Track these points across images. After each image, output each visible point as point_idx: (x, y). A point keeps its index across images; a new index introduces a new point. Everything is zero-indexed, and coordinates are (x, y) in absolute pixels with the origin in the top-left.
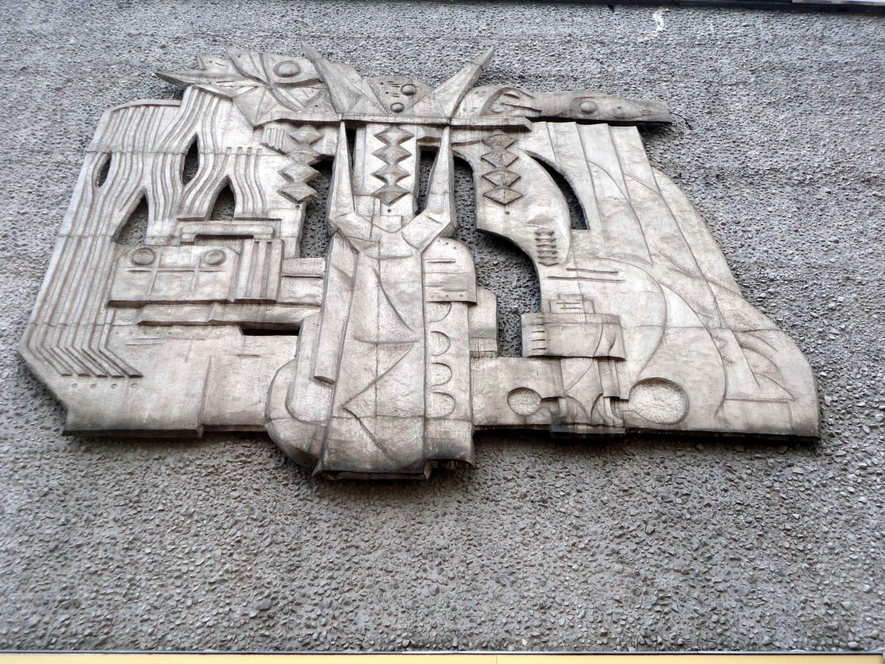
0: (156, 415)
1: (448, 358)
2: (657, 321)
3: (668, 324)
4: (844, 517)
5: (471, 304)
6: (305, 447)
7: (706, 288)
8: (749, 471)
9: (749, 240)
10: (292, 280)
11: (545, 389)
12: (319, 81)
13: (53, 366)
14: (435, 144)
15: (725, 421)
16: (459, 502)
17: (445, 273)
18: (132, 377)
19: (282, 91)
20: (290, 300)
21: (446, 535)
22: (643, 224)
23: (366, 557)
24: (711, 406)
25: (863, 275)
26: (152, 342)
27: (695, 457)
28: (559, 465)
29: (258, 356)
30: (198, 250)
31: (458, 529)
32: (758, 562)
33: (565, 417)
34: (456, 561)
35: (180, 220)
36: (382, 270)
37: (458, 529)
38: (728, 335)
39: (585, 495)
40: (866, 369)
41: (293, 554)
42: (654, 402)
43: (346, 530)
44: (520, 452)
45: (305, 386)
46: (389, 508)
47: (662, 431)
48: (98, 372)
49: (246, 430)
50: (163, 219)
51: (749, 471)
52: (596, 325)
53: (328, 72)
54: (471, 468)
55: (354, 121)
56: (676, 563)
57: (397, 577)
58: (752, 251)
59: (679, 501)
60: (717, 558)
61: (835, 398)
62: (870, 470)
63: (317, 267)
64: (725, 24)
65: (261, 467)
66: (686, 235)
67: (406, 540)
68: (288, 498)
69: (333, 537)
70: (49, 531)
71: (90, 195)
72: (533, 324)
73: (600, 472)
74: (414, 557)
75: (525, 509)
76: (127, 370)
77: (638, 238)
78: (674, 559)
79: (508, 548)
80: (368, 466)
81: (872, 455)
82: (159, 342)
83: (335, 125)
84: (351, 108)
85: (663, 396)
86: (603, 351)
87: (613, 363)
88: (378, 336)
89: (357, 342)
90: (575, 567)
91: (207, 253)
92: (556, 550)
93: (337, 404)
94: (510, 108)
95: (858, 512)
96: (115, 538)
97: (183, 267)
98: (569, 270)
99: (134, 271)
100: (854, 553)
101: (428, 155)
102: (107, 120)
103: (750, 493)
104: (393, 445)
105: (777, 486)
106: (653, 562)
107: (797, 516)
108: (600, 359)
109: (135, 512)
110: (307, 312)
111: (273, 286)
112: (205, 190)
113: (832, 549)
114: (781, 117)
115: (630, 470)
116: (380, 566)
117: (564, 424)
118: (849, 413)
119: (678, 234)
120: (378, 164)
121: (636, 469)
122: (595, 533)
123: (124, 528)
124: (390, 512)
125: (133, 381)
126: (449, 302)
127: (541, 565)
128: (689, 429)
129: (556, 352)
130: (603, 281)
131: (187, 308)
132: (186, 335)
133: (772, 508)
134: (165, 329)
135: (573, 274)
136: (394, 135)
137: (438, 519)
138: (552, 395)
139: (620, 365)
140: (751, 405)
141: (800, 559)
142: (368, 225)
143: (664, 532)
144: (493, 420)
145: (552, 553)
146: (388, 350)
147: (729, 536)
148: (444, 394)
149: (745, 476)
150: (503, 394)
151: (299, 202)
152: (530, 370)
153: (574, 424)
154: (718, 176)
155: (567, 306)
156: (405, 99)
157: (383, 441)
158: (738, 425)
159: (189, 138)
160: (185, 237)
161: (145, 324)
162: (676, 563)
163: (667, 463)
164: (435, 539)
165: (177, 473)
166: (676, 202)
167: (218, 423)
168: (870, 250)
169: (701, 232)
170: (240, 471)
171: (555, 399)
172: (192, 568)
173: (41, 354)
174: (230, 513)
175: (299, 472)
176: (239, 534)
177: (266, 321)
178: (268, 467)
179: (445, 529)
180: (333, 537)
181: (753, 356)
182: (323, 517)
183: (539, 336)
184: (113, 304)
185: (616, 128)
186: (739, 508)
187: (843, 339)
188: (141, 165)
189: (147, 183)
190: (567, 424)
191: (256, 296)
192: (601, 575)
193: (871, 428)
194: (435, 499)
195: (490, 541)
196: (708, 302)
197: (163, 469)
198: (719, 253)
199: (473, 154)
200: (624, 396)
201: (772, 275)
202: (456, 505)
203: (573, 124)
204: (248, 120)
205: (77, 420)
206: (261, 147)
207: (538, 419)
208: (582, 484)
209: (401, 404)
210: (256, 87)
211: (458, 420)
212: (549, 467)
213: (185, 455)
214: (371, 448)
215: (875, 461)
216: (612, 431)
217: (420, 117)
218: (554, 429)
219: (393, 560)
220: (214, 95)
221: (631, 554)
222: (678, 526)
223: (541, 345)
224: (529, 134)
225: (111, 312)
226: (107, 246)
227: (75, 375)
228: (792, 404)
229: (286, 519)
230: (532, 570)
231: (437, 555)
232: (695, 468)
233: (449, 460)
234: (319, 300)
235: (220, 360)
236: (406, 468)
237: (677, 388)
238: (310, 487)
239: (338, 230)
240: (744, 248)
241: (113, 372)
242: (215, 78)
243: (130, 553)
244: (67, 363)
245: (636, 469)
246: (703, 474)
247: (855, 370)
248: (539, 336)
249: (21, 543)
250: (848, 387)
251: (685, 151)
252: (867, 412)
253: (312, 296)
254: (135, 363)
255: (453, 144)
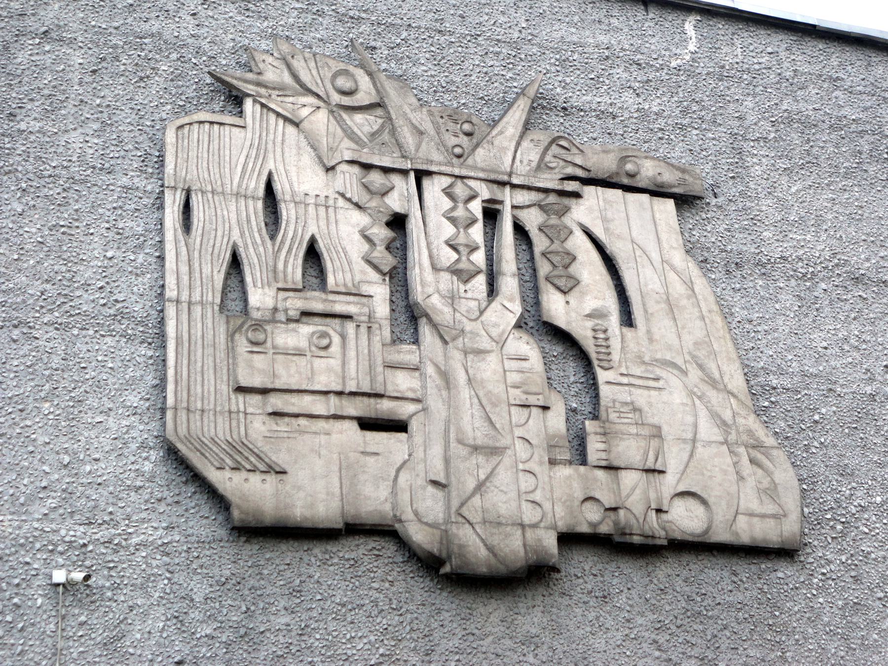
0: (308, 513)
1: (532, 466)
2: (690, 436)
3: (698, 436)
4: (807, 615)
5: (545, 408)
6: (435, 551)
7: (727, 401)
8: (747, 575)
9: (758, 342)
10: (393, 370)
11: (608, 500)
12: (378, 105)
13: (206, 458)
14: (497, 207)
15: (737, 534)
16: (544, 596)
17: (523, 372)
18: (277, 473)
19: (345, 116)
20: (396, 394)
21: (536, 624)
22: (679, 326)
23: (481, 642)
24: (728, 520)
25: (842, 386)
26: (286, 435)
27: (710, 561)
28: (614, 564)
29: (377, 454)
30: (306, 329)
31: (545, 620)
32: (749, 651)
33: (624, 528)
34: (545, 647)
35: (279, 289)
36: (469, 364)
37: (545, 620)
38: (742, 450)
39: (633, 592)
40: (835, 483)
41: (427, 639)
42: (686, 513)
43: (464, 619)
44: (585, 552)
45: (424, 488)
46: (493, 600)
47: (693, 542)
48: (248, 467)
49: (379, 528)
50: (263, 287)
51: (747, 575)
52: (645, 437)
53: (388, 95)
54: (555, 569)
55: (422, 171)
56: (695, 652)
57: (505, 660)
58: (761, 355)
59: (699, 599)
60: (723, 647)
61: (811, 510)
62: (828, 575)
63: (413, 357)
64: (751, 48)
65: (391, 560)
66: (712, 340)
67: (508, 628)
68: (418, 590)
69: (455, 625)
70: (235, 618)
71: (184, 249)
72: (596, 434)
73: (643, 572)
74: (516, 643)
75: (591, 603)
76: (273, 465)
77: (676, 342)
78: (695, 647)
79: (581, 636)
80: (485, 570)
81: (831, 562)
82: (291, 435)
83: (404, 172)
84: (417, 150)
85: (693, 508)
86: (650, 464)
87: (656, 474)
88: (475, 439)
89: (460, 446)
90: (628, 653)
91: (313, 333)
92: (614, 640)
93: (453, 509)
94: (562, 163)
95: (817, 611)
96: (289, 625)
97: (295, 349)
98: (622, 375)
99: (252, 352)
100: (811, 644)
101: (491, 215)
102: (174, 140)
103: (748, 594)
104: (501, 550)
105: (765, 587)
106: (680, 650)
107: (777, 613)
108: (648, 471)
109: (299, 601)
110: (411, 408)
111: (380, 378)
112: (294, 250)
113: (797, 640)
114: (793, 190)
115: (667, 571)
116: (492, 651)
117: (624, 534)
118: (819, 524)
119: (707, 339)
120: (449, 230)
121: (670, 571)
122: (641, 625)
123: (294, 615)
124: (494, 604)
125: (280, 476)
126: (529, 406)
127: (605, 651)
128: (712, 541)
129: (616, 463)
130: (648, 388)
131: (308, 398)
132: (314, 429)
133: (761, 607)
134: (293, 420)
135: (625, 380)
136: (460, 190)
137: (530, 611)
138: (613, 506)
139: (661, 475)
140: (755, 520)
141: (776, 648)
142: (451, 310)
143: (688, 625)
144: (572, 528)
145: (611, 642)
146: (486, 454)
147: (731, 629)
148: (533, 502)
149: (745, 579)
150: (577, 503)
151: (385, 274)
152: (595, 480)
153: (631, 534)
154: (737, 264)
155: (622, 415)
156: (464, 140)
157: (493, 546)
158: (745, 539)
159: (264, 178)
160: (291, 313)
161: (277, 414)
162: (695, 652)
163: (692, 566)
164: (529, 628)
165: (324, 564)
166: (705, 300)
167: (357, 522)
168: (850, 360)
169: (724, 338)
170: (375, 564)
171: (615, 509)
172: (354, 652)
173: (192, 444)
174: (375, 603)
175: (422, 566)
176: (384, 622)
177: (380, 417)
178: (395, 560)
179: (535, 620)
180: (455, 625)
181: (760, 472)
182: (446, 607)
183: (602, 446)
184: (241, 390)
185: (656, 200)
186: (739, 606)
187: (821, 453)
188: (225, 213)
189: (236, 236)
190: (625, 534)
191: (366, 389)
192: (645, 660)
193: (833, 538)
194: (525, 592)
195: (568, 630)
196: (727, 415)
197: (313, 559)
198: (737, 364)
199: (532, 220)
200: (665, 508)
201: (775, 382)
202: (542, 598)
203: (619, 192)
204: (320, 158)
205: (243, 516)
206: (337, 196)
207: (604, 529)
208: (626, 580)
209: (503, 511)
210: (318, 108)
211: (547, 528)
212: (607, 566)
213: (329, 547)
214: (483, 552)
215: (833, 567)
216: (659, 542)
217: (483, 170)
218: (617, 539)
219: (501, 646)
220: (278, 115)
221: (666, 643)
222: (698, 620)
223: (603, 455)
224: (581, 201)
225: (241, 397)
226: (217, 320)
227: (227, 468)
228: (783, 519)
229: (418, 609)
230: (599, 655)
231: (530, 640)
232: (711, 571)
233: (544, 567)
234: (419, 395)
235: (347, 458)
236: (514, 573)
237: (704, 502)
238: (432, 580)
239: (427, 315)
240: (754, 351)
241: (262, 467)
242: (274, 89)
243: (304, 638)
244: (217, 455)
245: (670, 571)
246: (714, 574)
247: (827, 484)
248: (602, 446)
249: (215, 629)
250: (821, 500)
251: (713, 227)
252: (832, 523)
253: (413, 390)
254: (280, 458)
255: (514, 207)
